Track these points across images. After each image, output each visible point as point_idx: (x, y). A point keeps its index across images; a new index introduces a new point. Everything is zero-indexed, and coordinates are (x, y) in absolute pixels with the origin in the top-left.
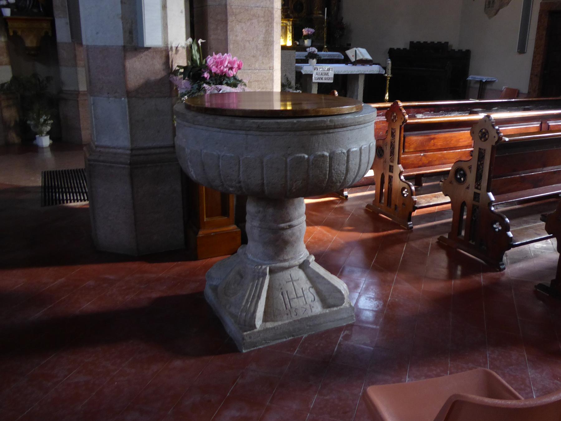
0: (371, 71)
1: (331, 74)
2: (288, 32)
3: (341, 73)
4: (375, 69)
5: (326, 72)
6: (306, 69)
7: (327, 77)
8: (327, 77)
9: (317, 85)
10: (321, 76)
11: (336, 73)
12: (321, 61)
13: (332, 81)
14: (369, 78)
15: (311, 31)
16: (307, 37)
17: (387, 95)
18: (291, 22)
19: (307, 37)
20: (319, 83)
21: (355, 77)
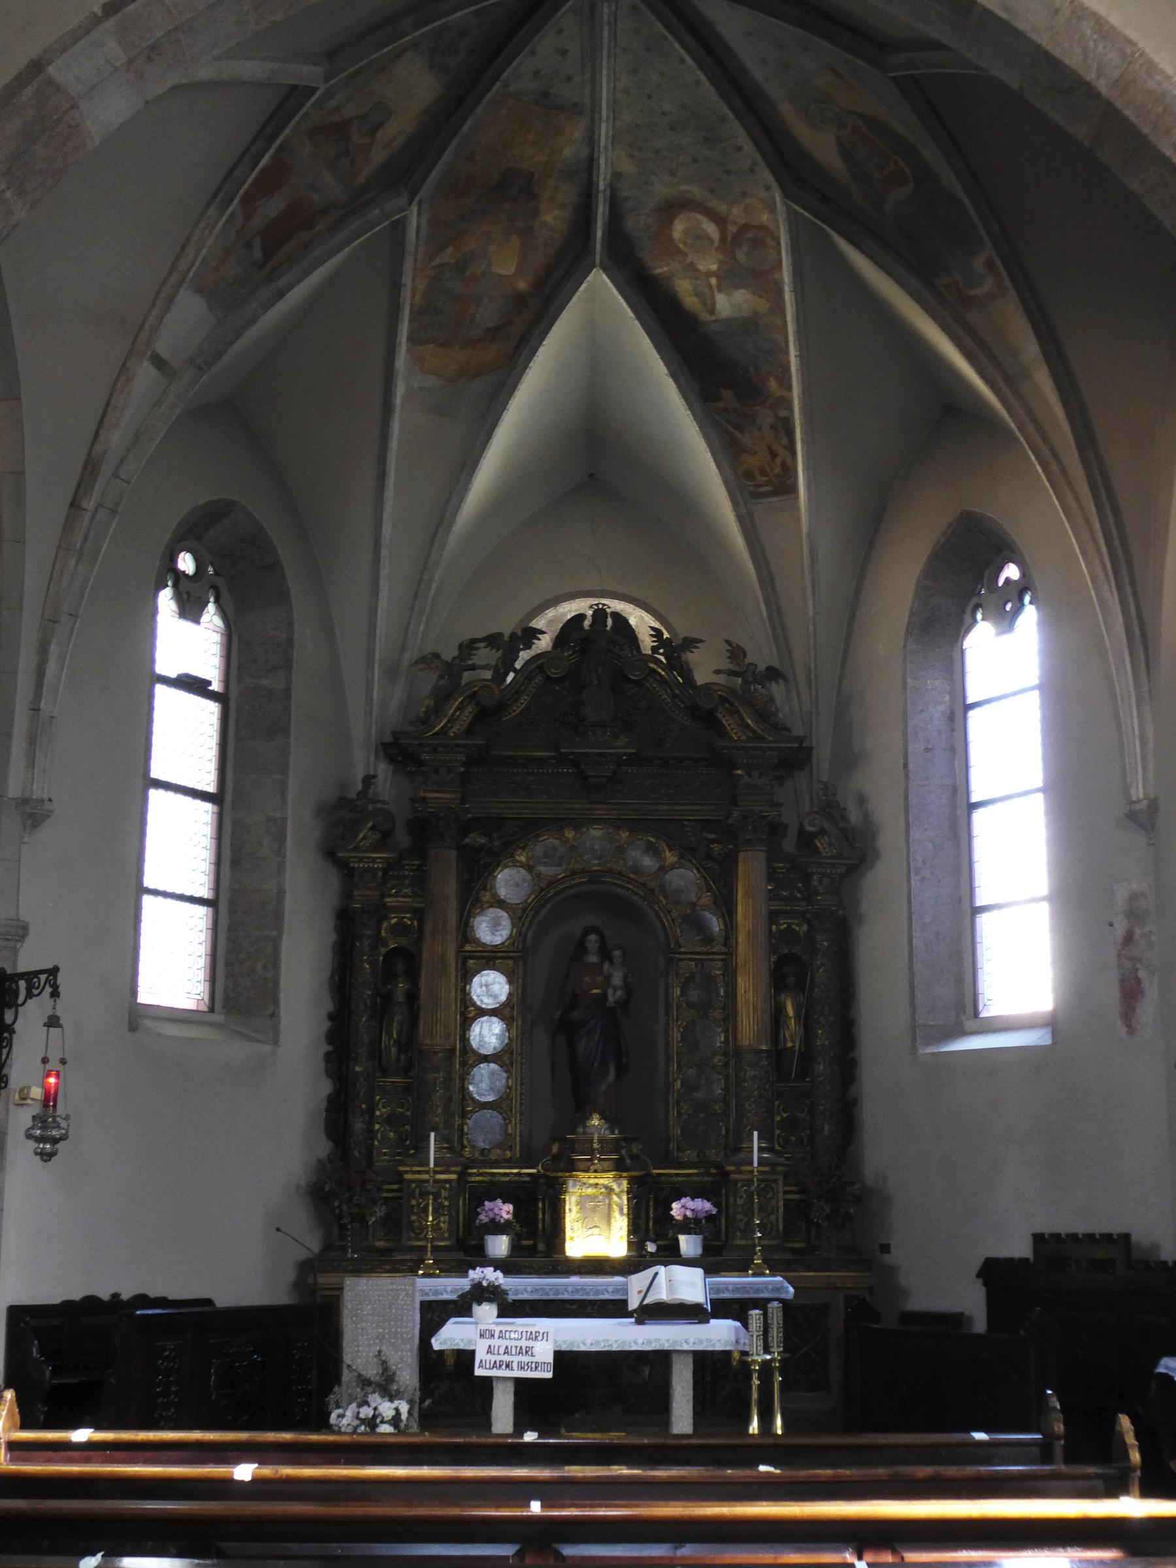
0: (572, 1343)
1: (544, 1352)
2: (616, 1214)
3: (583, 1348)
4: (720, 1334)
5: (524, 1343)
6: (453, 1335)
7: (526, 1359)
8: (526, 1359)
9: (510, 1388)
10: (506, 1358)
11: (564, 1348)
12: (511, 1309)
13: (549, 1375)
14: (708, 1365)
15: (703, 1205)
16: (688, 1226)
17: (779, 1422)
18: (625, 1183)
19: (688, 1226)
20: (520, 1383)
21: (661, 1360)
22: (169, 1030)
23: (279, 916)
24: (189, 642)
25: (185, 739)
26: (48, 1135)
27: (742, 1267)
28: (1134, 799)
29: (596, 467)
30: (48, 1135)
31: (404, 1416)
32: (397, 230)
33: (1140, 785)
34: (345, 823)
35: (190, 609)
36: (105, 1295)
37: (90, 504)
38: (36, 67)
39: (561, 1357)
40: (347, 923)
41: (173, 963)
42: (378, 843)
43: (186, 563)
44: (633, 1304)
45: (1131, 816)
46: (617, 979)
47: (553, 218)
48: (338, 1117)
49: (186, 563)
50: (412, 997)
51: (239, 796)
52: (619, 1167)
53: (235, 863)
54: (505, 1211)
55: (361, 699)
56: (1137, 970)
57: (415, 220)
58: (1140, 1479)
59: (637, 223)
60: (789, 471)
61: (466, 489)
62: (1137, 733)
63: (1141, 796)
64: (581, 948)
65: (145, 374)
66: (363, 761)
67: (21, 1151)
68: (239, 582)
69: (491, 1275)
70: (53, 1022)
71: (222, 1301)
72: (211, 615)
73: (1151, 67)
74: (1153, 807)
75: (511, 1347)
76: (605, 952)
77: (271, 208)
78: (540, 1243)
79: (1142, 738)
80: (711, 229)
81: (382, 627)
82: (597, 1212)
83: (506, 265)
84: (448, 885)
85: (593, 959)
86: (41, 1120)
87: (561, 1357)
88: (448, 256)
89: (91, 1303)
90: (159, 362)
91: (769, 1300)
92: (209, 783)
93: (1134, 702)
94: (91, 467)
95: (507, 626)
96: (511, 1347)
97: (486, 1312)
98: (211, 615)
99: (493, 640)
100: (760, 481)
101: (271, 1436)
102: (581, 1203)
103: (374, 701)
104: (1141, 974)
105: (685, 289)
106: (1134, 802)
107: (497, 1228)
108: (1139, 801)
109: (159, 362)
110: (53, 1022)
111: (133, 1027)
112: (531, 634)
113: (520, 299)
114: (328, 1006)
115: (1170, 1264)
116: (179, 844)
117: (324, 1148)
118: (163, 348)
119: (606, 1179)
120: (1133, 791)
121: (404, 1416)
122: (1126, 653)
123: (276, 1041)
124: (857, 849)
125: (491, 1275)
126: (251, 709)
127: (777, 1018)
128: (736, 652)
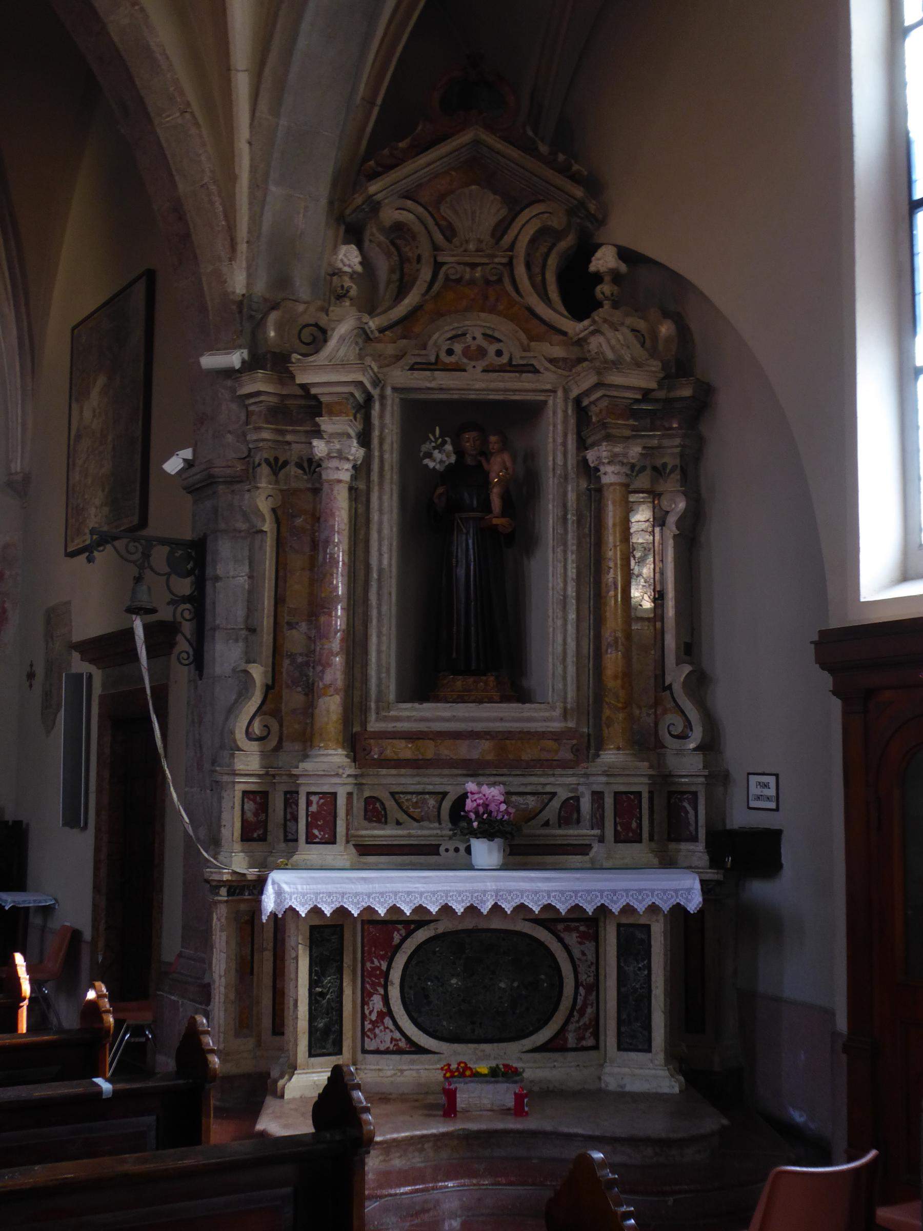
28: (13, 471)
31: (509, 464)
33: (19, 461)
44: (591, 455)
45: (10, 484)
56: (4, 602)
58: (28, 1007)
62: (20, 421)
63: (19, 470)
74: (27, 479)
79: (24, 424)
91: (470, 1076)
93: (19, 397)
101: (471, 552)
104: (8, 605)
106: (12, 474)
108: (16, 473)
115: (10, 823)
120: (13, 466)
121: (509, 464)
122: (17, 358)
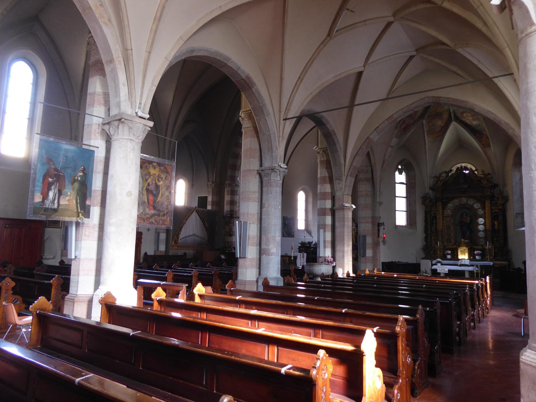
4: (471, 269)
6: (434, 267)
12: (442, 264)
15: (480, 252)
19: (477, 255)
22: (401, 228)
23: (416, 213)
24: (400, 178)
25: (401, 190)
26: (384, 242)
27: (486, 261)
29: (460, 145)
30: (384, 242)
32: (422, 123)
34: (425, 199)
35: (400, 173)
36: (394, 261)
37: (384, 166)
38: (368, 137)
39: (449, 270)
40: (426, 213)
41: (401, 219)
42: (429, 202)
43: (400, 167)
46: (469, 219)
47: (445, 116)
48: (426, 239)
49: (400, 167)
50: (436, 223)
51: (409, 197)
52: (467, 246)
53: (410, 206)
54: (449, 252)
55: (426, 182)
57: (424, 121)
59: (458, 115)
60: (489, 144)
61: (439, 153)
64: (463, 215)
65: (390, 149)
66: (428, 190)
67: (381, 244)
68: (407, 169)
69: (439, 260)
70: (384, 229)
71: (410, 262)
72: (404, 173)
73: (498, 117)
75: (442, 269)
76: (466, 215)
77: (403, 126)
78: (455, 257)
80: (469, 114)
81: (428, 171)
82: (463, 253)
83: (440, 123)
84: (440, 208)
85: (465, 216)
86: (383, 240)
87: (449, 270)
88: (430, 124)
89: (392, 262)
90: (391, 147)
92: (405, 195)
94: (384, 161)
95: (447, 170)
96: (442, 269)
97: (439, 264)
98: (404, 173)
99: (445, 172)
100: (486, 145)
102: (461, 251)
103: (428, 182)
105: (467, 121)
107: (448, 254)
109: (391, 147)
110: (384, 229)
111: (396, 228)
112: (451, 171)
113: (443, 126)
114: (424, 224)
116: (401, 204)
117: (425, 243)
118: (391, 145)
119: (465, 248)
123: (416, 229)
124: (506, 199)
125: (439, 260)
126: (410, 185)
127: (493, 225)
128: (483, 171)
